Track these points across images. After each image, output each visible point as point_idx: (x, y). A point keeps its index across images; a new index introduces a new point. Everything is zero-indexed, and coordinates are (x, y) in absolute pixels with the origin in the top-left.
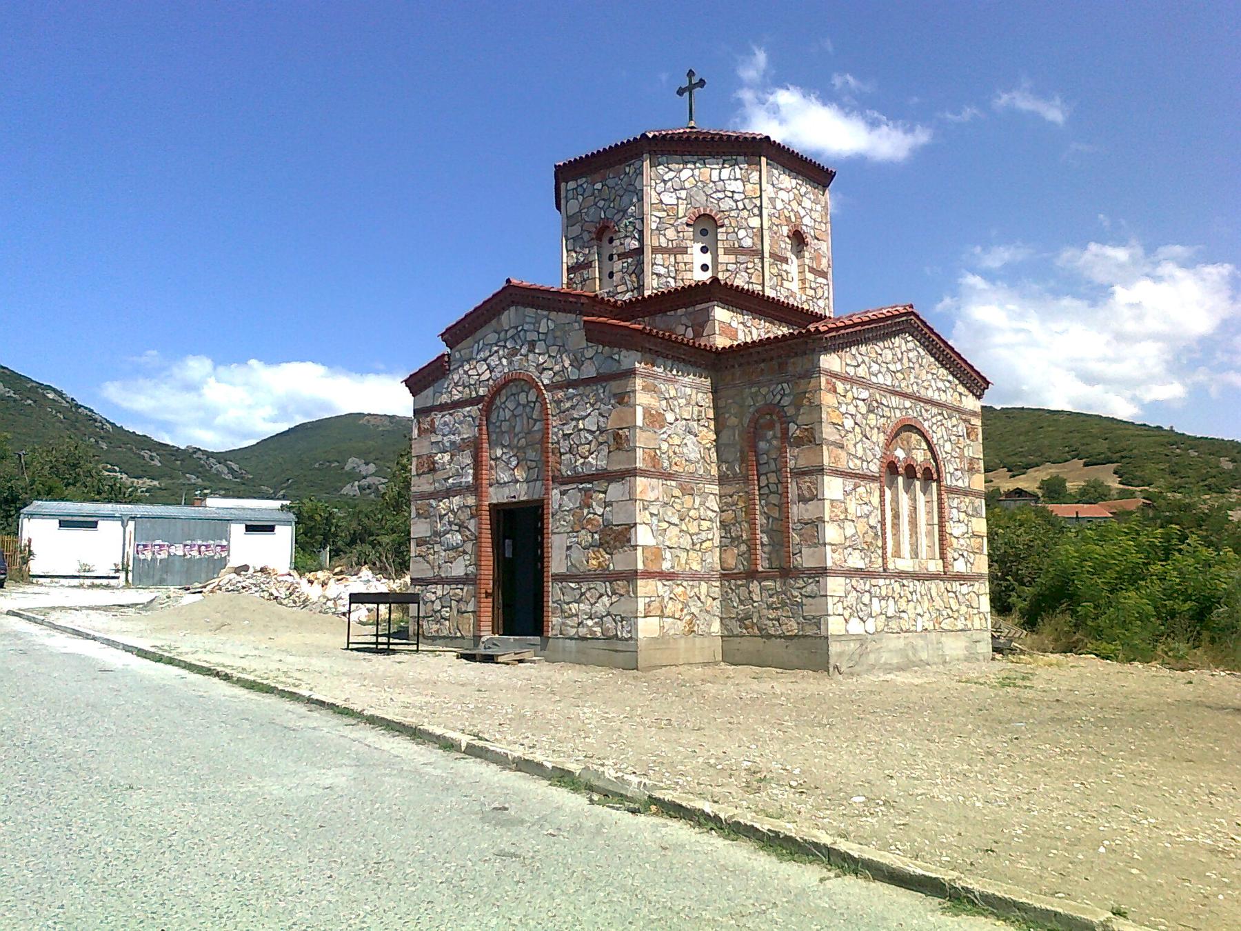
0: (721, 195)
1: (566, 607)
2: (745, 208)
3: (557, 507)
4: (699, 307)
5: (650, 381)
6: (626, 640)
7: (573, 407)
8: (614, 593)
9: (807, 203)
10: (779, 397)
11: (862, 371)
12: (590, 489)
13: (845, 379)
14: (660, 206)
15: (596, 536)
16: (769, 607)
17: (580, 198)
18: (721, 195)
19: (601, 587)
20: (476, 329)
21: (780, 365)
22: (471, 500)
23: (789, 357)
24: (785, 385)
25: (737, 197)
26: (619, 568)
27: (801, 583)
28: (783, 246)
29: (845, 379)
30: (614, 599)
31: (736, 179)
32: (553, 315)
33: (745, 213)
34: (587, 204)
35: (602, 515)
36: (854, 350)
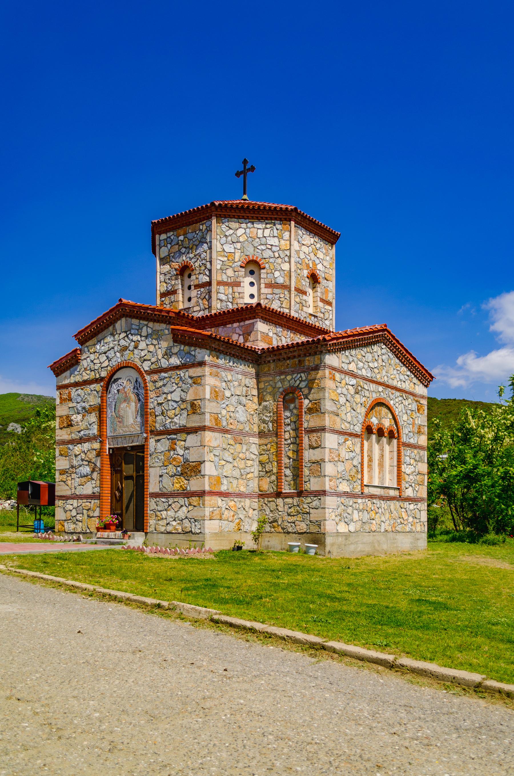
2: (279, 257)
3: (153, 450)
4: (247, 322)
7: (164, 385)
8: (190, 504)
10: (298, 382)
11: (352, 367)
12: (175, 439)
13: (341, 371)
15: (179, 469)
16: (289, 515)
17: (169, 246)
18: (263, 247)
19: (181, 501)
21: (299, 361)
23: (305, 355)
24: (303, 375)
25: (274, 249)
27: (309, 500)
29: (341, 371)
30: (190, 508)
31: (274, 237)
32: (151, 324)
33: (279, 260)
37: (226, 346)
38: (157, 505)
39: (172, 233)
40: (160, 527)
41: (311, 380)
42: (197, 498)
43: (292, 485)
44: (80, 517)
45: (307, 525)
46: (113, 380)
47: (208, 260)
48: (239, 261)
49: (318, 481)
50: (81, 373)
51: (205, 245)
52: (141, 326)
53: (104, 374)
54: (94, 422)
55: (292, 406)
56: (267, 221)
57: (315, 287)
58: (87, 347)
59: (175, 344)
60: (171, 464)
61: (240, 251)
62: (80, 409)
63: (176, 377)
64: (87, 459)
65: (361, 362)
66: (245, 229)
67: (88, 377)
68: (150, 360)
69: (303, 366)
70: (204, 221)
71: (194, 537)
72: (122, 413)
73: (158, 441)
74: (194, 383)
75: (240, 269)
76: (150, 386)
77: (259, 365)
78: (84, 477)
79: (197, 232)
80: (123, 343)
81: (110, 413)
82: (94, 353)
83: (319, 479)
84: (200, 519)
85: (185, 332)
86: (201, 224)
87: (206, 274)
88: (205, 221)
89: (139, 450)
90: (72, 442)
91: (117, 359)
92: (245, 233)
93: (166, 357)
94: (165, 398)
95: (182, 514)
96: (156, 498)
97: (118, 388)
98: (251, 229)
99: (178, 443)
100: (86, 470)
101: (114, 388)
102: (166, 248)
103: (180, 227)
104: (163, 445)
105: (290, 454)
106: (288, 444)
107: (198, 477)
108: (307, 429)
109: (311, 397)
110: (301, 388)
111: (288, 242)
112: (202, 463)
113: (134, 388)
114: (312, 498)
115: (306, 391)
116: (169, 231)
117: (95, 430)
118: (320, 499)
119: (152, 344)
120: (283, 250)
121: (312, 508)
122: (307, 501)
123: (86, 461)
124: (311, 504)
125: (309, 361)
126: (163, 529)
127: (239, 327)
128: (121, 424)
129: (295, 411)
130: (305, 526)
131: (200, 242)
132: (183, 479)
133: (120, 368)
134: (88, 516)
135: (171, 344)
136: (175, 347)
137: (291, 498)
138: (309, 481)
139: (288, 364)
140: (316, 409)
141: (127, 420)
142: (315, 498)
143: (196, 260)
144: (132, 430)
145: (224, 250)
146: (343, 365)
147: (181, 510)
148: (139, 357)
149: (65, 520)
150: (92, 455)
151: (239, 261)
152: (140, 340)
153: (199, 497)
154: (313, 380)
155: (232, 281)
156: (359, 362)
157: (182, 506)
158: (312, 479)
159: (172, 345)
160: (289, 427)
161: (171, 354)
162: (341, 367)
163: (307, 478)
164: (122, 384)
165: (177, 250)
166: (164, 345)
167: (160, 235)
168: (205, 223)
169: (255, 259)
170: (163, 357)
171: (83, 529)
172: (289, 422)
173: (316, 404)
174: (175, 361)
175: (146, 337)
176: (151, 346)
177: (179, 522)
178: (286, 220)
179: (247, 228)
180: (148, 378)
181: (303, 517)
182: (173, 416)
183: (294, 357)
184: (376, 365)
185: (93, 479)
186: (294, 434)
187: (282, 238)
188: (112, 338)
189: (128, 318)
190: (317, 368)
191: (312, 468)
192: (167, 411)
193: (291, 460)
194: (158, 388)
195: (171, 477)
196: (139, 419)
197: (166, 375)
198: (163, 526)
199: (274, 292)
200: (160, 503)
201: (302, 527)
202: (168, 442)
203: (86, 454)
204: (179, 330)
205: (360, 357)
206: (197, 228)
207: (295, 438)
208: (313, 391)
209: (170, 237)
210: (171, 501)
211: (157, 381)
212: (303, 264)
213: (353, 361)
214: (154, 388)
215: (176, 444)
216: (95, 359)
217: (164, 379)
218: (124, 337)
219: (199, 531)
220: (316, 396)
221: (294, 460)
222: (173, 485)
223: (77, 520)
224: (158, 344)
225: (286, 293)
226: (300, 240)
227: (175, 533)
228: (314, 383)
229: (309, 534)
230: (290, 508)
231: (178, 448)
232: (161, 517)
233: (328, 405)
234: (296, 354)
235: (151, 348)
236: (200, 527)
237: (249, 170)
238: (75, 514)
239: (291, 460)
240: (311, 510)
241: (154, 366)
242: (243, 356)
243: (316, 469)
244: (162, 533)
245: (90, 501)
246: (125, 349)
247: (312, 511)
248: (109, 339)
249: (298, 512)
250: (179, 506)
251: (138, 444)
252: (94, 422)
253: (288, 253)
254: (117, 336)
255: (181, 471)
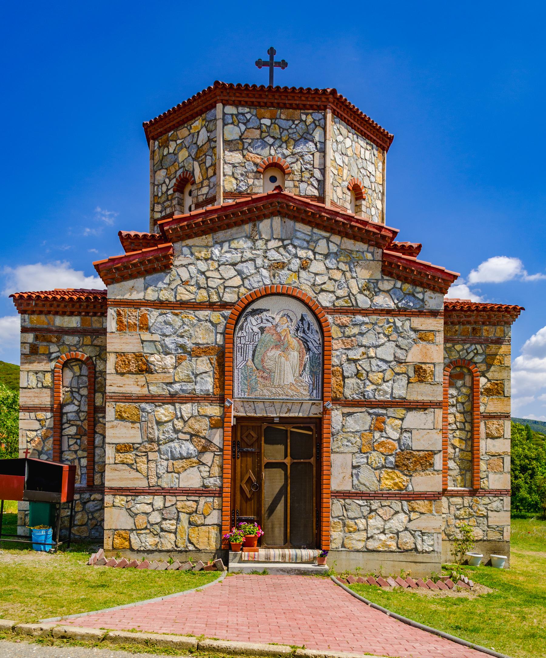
1: (351, 523)
3: (339, 427)
6: (428, 552)
7: (361, 334)
8: (413, 510)
10: (472, 355)
12: (383, 415)
15: (392, 459)
16: (457, 518)
17: (243, 127)
19: (396, 505)
20: (221, 228)
21: (474, 329)
22: (214, 411)
23: (484, 324)
24: (478, 347)
26: (418, 489)
27: (486, 500)
30: (413, 516)
32: (336, 239)
35: (399, 440)
38: (346, 510)
39: (247, 110)
40: (354, 542)
41: (489, 355)
42: (426, 502)
43: (459, 481)
44: (172, 525)
45: (484, 531)
46: (249, 310)
47: (317, 164)
49: (500, 478)
50: (173, 286)
51: (311, 143)
52: (315, 238)
53: (229, 297)
54: (206, 372)
55: (460, 383)
56: (369, 142)
58: (190, 247)
59: (385, 277)
60: (374, 450)
62: (172, 346)
63: (387, 326)
64: (190, 430)
67: (192, 296)
68: (333, 292)
69: (479, 336)
70: (308, 109)
71: (420, 558)
72: (269, 364)
73: (349, 414)
74: (420, 339)
76: (335, 332)
78: (181, 459)
79: (296, 122)
80: (273, 255)
81: (240, 363)
82: (206, 260)
83: (501, 476)
84: (433, 531)
85: (412, 264)
86: (303, 113)
87: (312, 185)
88: (311, 111)
89: (298, 425)
90: (151, 399)
91: (263, 279)
93: (367, 293)
94: (363, 354)
95: (397, 524)
96: (344, 499)
97: (262, 325)
99: (388, 421)
100: (189, 448)
101: (252, 323)
102: (237, 129)
103: (265, 105)
104: (361, 421)
105: (456, 442)
106: (452, 430)
107: (428, 472)
108: (484, 414)
109: (489, 375)
110: (476, 363)
112: (435, 454)
113: (297, 330)
114: (491, 498)
115: (483, 367)
116: (243, 106)
117: (208, 384)
118: (502, 500)
119: (338, 269)
121: (492, 511)
122: (484, 502)
123: (185, 433)
124: (490, 505)
125: (487, 331)
126: (360, 546)
128: (267, 382)
129: (464, 390)
130: (481, 533)
131: (302, 137)
132: (400, 474)
133: (269, 293)
134: (190, 523)
135: (378, 276)
136: (385, 282)
137: (460, 496)
138: (487, 477)
139: (456, 331)
140: (498, 390)
141: (280, 379)
142: (495, 499)
143: (294, 160)
144: (291, 393)
147: (395, 518)
148: (310, 284)
149: (132, 530)
150: (202, 426)
152: (312, 257)
153: (430, 500)
154: (493, 355)
157: (397, 512)
158: (491, 476)
159: (380, 278)
160: (454, 408)
161: (376, 290)
163: (484, 473)
164: (270, 319)
166: (363, 274)
167: (224, 105)
168: (311, 114)
170: (361, 292)
171: (179, 545)
172: (455, 403)
173: (497, 384)
174: (384, 301)
175: (326, 256)
176: (336, 271)
177: (391, 535)
180: (330, 318)
181: (478, 521)
182: (380, 381)
183: (469, 323)
185: (204, 464)
186: (462, 418)
188: (249, 244)
189: (286, 220)
190: (499, 342)
191: (491, 461)
192: (368, 372)
193: (457, 450)
194: (349, 337)
195: (376, 469)
196: (306, 378)
197: (366, 319)
198: (360, 540)
200: (354, 506)
201: (477, 533)
202: (369, 418)
203: (185, 422)
204: (399, 258)
206: (296, 117)
207: (464, 423)
208: (493, 368)
209: (243, 114)
210: (375, 505)
211: (346, 326)
214: (340, 335)
215: (384, 423)
216: (208, 270)
217: (361, 325)
218: (278, 248)
219: (431, 549)
220: (497, 376)
221: (461, 450)
222: (379, 481)
223: (162, 530)
224: (351, 271)
227: (385, 551)
228: (494, 359)
229: (486, 542)
230: (458, 509)
231: (388, 429)
232: (355, 527)
233: (513, 389)
234: (472, 319)
235: (337, 275)
236: (432, 543)
237: (278, 64)
238: (159, 520)
239: (457, 450)
240: (489, 513)
241: (340, 303)
243: (496, 463)
244: (358, 551)
245: (197, 498)
246: (281, 265)
247: (490, 513)
248: (243, 244)
249: (470, 514)
250: (392, 512)
251: (301, 415)
252: (206, 372)
254: (260, 243)
255: (396, 462)
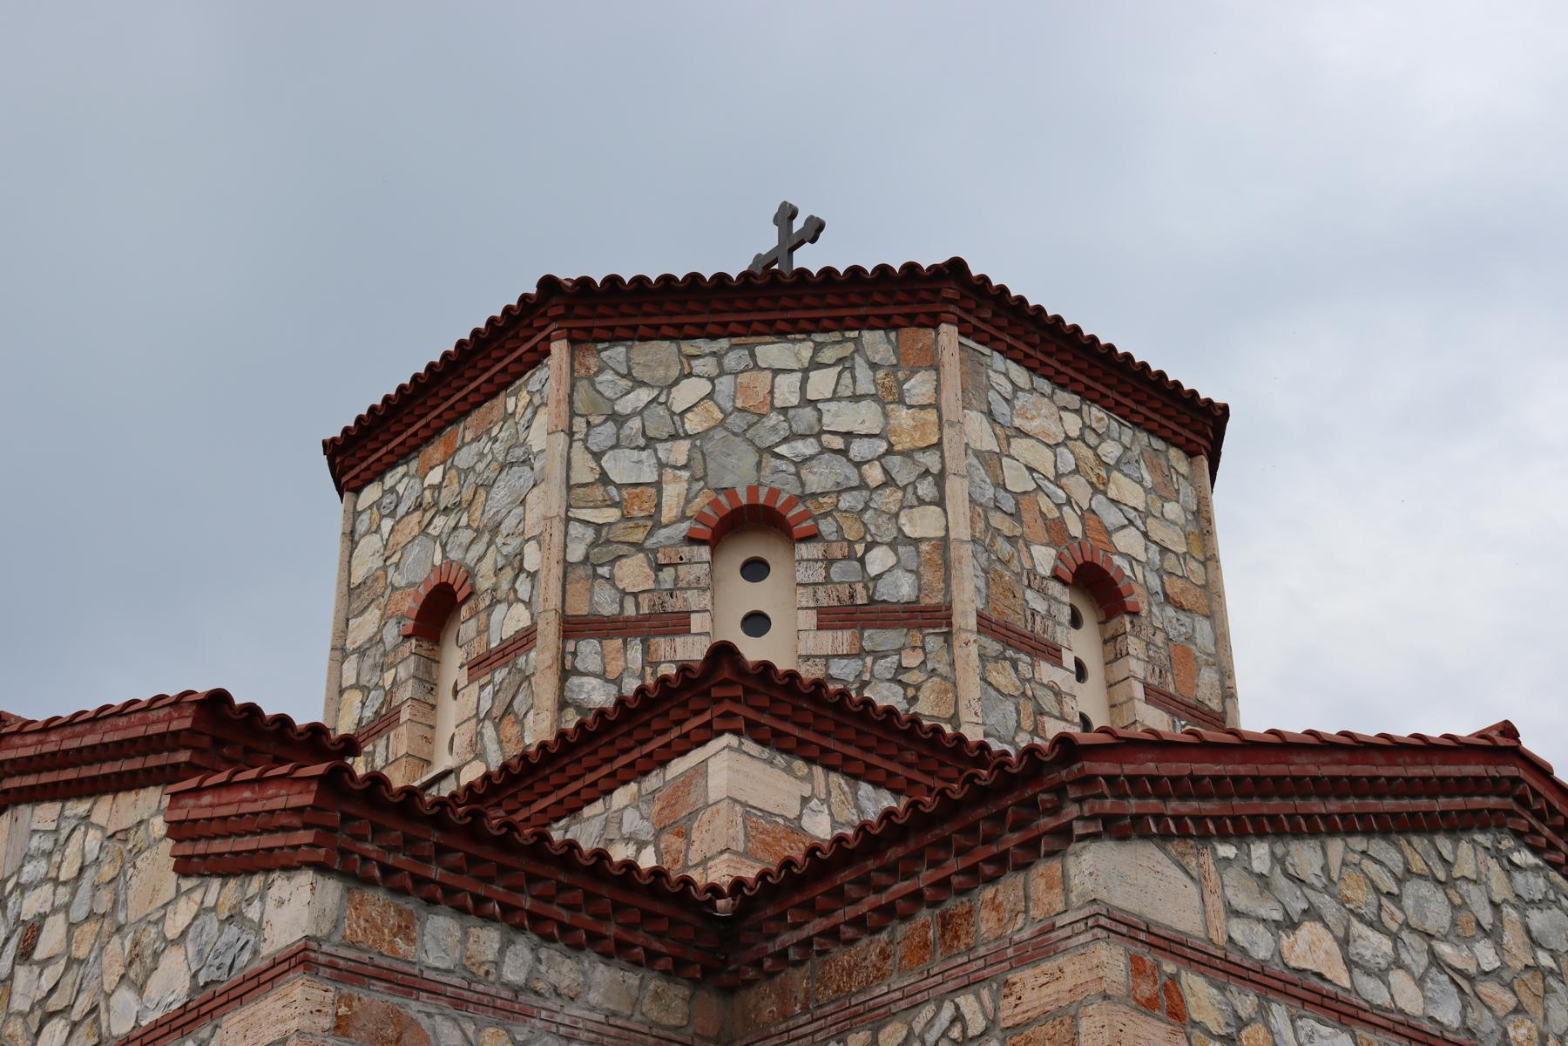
0: (807, 448)
2: (889, 481)
4: (678, 767)
5: (375, 998)
9: (1133, 495)
11: (1311, 950)
13: (1229, 968)
14: (598, 493)
18: (807, 448)
21: (945, 922)
24: (967, 1003)
25: (859, 449)
28: (1039, 605)
29: (1229, 968)
31: (856, 398)
33: (889, 499)
34: (402, 539)
36: (1260, 853)
37: (471, 860)
48: (683, 517)
57: (1114, 638)
59: (187, 884)
61: (685, 474)
65: (1376, 925)
66: (711, 380)
75: (686, 551)
77: (728, 991)
92: (710, 396)
98: (744, 378)
111: (932, 416)
120: (908, 454)
127: (634, 804)
145: (604, 479)
146: (1238, 930)
151: (683, 517)
155: (645, 610)
156: (1358, 928)
162: (1221, 939)
165: (416, 530)
169: (762, 500)
178: (912, 320)
179: (722, 373)
184: (1487, 957)
187: (901, 401)
199: (867, 645)
205: (1362, 897)
209: (392, 490)
212: (1026, 517)
213: (1311, 913)
225: (934, 643)
226: (1001, 408)
242: (611, 930)
253: (931, 461)
